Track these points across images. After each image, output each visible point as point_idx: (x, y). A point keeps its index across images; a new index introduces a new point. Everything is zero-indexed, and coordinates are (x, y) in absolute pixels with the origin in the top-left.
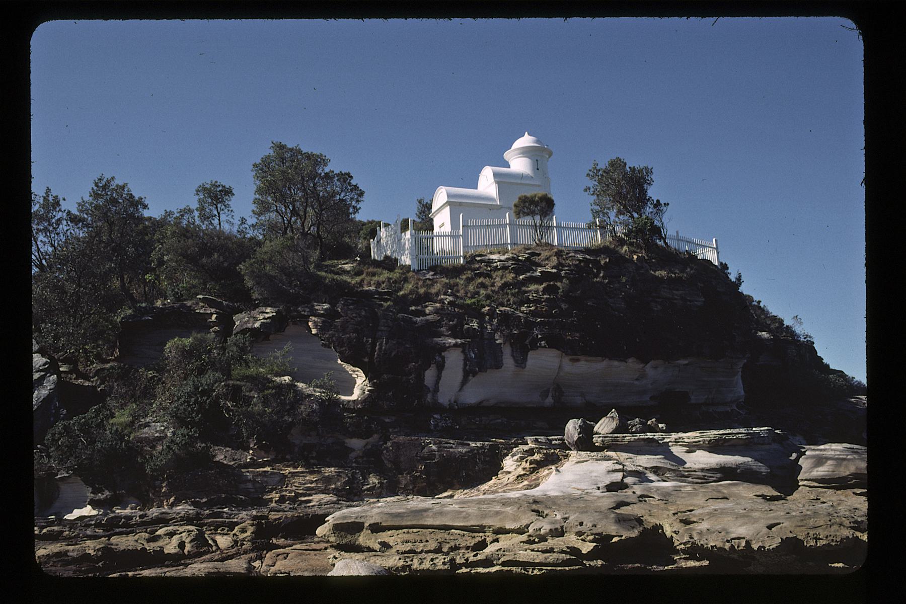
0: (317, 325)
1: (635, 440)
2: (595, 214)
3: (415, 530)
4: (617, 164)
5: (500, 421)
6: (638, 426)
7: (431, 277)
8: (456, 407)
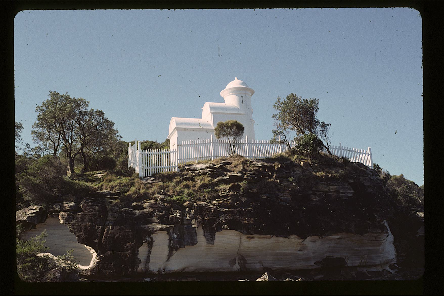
2: (276, 133)
7: (151, 182)
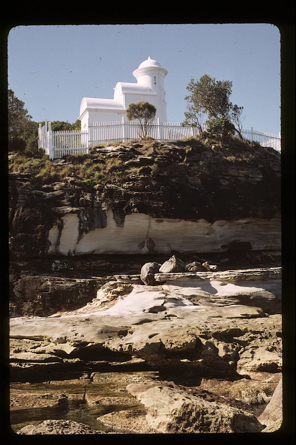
2: (188, 116)
4: (206, 79)
5: (104, 264)
6: (194, 267)
7: (61, 164)
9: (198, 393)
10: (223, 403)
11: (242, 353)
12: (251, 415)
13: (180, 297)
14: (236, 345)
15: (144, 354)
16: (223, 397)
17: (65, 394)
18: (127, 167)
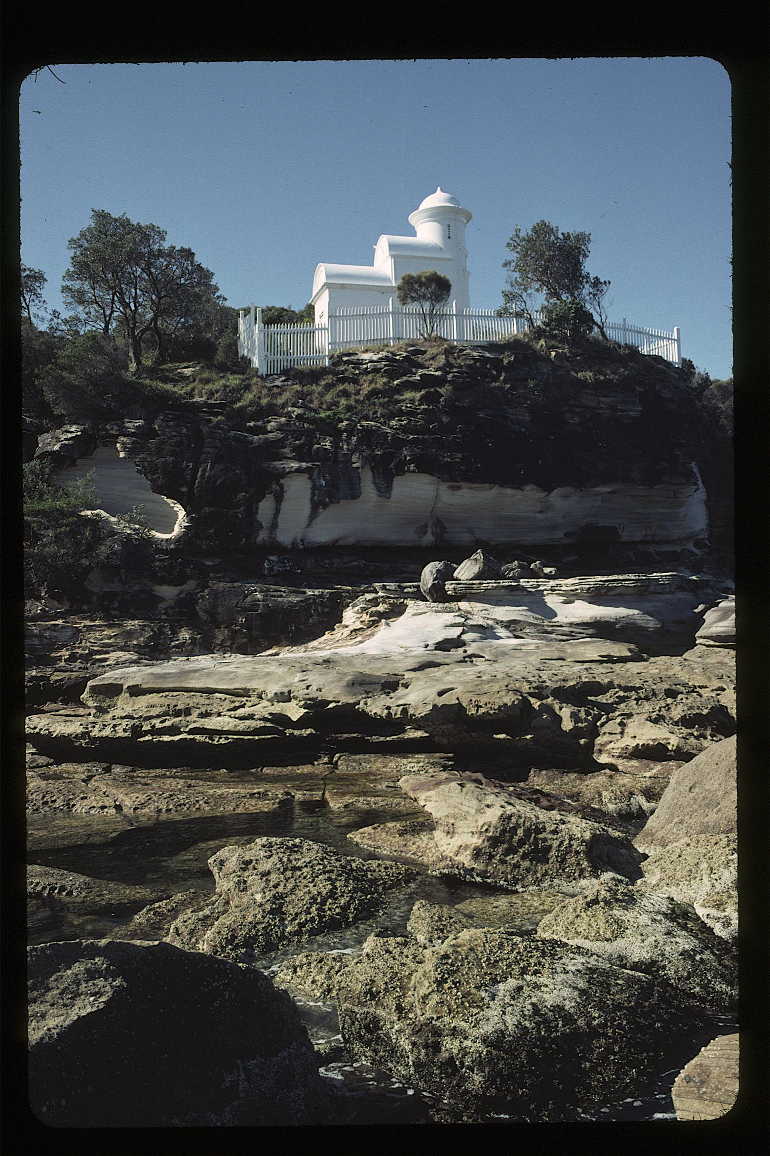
0: (126, 447)
1: (494, 588)
2: (509, 297)
3: (175, 694)
4: (543, 230)
5: (356, 563)
7: (280, 384)
8: (301, 547)
9: (525, 794)
10: (570, 811)
11: (603, 725)
12: (621, 835)
13: (490, 622)
14: (593, 710)
15: (429, 723)
16: (569, 801)
17: (290, 791)
18: (399, 389)
